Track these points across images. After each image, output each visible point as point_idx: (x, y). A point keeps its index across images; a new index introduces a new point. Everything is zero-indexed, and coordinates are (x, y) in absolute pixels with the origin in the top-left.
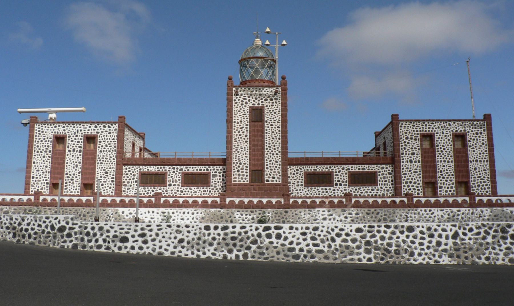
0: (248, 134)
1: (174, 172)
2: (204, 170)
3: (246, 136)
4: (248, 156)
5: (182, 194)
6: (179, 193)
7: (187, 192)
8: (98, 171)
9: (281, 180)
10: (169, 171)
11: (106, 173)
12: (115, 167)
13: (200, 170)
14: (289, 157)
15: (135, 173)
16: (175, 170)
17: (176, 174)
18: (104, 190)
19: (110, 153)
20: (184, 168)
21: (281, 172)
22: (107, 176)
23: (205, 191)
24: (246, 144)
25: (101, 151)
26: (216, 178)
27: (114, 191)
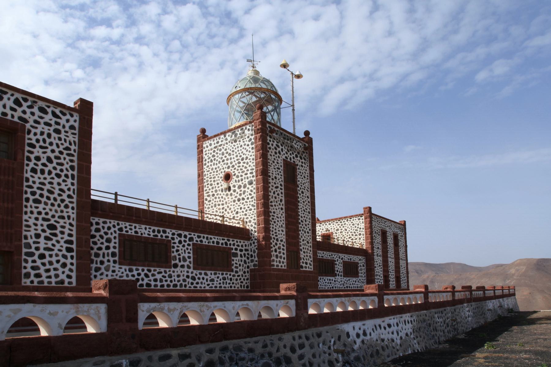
0: (283, 198)
1: (180, 242)
2: (222, 244)
3: (281, 201)
4: (284, 230)
7: (201, 280)
8: (29, 219)
9: (312, 267)
11: (52, 227)
12: (74, 216)
14: (92, 197)
15: (109, 236)
16: (183, 239)
18: (48, 271)
19: (60, 180)
21: (312, 256)
22: (55, 235)
23: (224, 279)
24: (282, 211)
25: (34, 171)
26: (237, 258)
27: (74, 275)
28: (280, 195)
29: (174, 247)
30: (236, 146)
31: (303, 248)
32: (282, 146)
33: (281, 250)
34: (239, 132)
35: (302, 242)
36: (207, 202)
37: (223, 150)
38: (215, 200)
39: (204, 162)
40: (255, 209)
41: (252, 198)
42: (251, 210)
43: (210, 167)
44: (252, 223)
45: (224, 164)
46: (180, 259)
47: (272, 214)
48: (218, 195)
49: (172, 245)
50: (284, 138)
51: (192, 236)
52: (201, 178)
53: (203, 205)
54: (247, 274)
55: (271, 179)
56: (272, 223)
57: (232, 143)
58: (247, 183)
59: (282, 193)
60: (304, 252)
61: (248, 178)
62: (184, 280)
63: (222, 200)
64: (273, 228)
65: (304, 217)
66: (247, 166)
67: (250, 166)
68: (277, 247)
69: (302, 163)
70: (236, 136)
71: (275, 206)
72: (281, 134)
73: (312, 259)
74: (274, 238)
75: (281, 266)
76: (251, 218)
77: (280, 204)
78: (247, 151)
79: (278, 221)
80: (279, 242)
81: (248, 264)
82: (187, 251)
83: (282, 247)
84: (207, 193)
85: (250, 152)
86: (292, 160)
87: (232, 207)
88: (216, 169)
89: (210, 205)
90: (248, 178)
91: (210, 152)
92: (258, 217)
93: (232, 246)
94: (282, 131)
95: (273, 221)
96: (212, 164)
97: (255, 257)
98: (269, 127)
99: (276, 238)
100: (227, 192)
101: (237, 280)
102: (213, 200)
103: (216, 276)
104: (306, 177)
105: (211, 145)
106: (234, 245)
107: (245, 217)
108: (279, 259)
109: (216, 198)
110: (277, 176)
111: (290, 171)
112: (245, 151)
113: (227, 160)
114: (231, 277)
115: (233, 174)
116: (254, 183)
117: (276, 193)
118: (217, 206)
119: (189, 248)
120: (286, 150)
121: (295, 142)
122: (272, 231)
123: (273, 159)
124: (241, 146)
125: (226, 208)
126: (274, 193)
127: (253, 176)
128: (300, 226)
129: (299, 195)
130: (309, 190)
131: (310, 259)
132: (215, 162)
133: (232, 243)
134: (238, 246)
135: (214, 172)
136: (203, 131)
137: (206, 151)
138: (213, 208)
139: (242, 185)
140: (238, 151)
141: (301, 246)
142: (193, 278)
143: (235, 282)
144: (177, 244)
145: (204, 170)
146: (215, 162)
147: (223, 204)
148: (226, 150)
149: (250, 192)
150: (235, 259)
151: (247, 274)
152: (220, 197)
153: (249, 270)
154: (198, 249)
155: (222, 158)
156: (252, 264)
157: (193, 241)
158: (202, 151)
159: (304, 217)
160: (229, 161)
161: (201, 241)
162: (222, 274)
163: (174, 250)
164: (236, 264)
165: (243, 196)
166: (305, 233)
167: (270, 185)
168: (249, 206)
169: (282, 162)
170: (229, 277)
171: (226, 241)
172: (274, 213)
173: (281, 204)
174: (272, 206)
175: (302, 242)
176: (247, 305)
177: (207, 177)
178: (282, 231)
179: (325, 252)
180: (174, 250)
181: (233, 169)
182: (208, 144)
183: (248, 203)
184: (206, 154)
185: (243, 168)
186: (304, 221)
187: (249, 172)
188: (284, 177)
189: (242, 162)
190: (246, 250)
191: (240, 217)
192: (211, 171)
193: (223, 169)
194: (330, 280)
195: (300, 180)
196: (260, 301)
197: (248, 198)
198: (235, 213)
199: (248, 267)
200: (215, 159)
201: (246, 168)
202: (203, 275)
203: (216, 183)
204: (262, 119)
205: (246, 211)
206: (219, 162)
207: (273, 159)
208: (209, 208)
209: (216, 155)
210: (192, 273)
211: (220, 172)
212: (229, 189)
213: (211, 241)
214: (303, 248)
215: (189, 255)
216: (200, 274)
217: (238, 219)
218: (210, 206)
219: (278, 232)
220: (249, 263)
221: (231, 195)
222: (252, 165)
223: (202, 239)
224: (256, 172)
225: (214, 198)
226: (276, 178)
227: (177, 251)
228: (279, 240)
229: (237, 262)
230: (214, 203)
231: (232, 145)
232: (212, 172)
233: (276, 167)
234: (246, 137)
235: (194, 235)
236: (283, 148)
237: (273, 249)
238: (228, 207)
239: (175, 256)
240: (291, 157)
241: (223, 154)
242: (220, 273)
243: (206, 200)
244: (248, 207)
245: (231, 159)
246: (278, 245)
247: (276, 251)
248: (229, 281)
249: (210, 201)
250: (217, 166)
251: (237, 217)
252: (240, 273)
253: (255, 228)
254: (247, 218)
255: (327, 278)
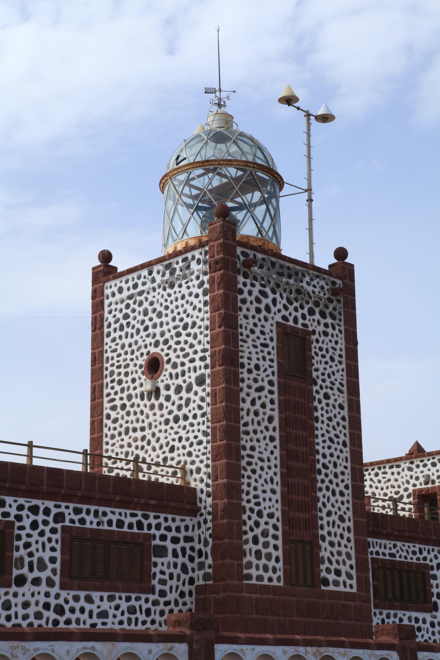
0: (276, 414)
1: (34, 525)
2: (131, 526)
3: (271, 419)
4: (278, 489)
5: (62, 619)
6: (52, 615)
7: (78, 614)
9: (354, 582)
10: (19, 518)
13: (120, 524)
16: (41, 517)
17: (42, 534)
20: (68, 509)
21: (353, 553)
23: (132, 610)
24: (271, 445)
26: (165, 560)
28: (269, 406)
29: (19, 538)
30: (173, 297)
31: (329, 534)
32: (274, 292)
33: (270, 539)
34: (178, 264)
35: (326, 519)
36: (109, 423)
37: (146, 305)
38: (126, 418)
39: (106, 330)
40: (208, 442)
41: (203, 415)
42: (200, 443)
43: (118, 341)
44: (202, 475)
45: (148, 336)
46: (31, 565)
47: (248, 452)
48: (132, 406)
49: (17, 532)
50: (281, 274)
51: (63, 509)
52: (97, 366)
53: (102, 430)
54: (187, 599)
55: (245, 370)
56: (246, 474)
57: (165, 289)
58: (193, 380)
59: (272, 402)
60: (332, 544)
61: (195, 370)
62: (38, 615)
63: (141, 418)
64: (249, 485)
65: (332, 455)
66: (195, 342)
67: (200, 342)
68: (258, 531)
69: (326, 325)
70: (172, 273)
71: (255, 432)
72: (273, 264)
73: (353, 562)
74: (252, 510)
75: (270, 580)
76: (201, 462)
77: (267, 428)
78: (194, 308)
79: (262, 469)
80: (265, 518)
81: (191, 574)
82: (48, 546)
83: (272, 531)
84: (110, 401)
85: (200, 310)
86: (301, 321)
87: (162, 435)
88: (130, 345)
89: (115, 429)
90: (195, 371)
91: (119, 306)
92: (213, 460)
93: (153, 531)
94: (274, 259)
95: (249, 468)
96: (123, 334)
97: (207, 557)
98: (243, 253)
99: (256, 508)
100: (153, 400)
101: (162, 613)
102: (123, 418)
103: (113, 604)
104: (337, 358)
105: (120, 290)
106: (158, 527)
107: (189, 459)
108: (264, 561)
109: (128, 414)
110: (261, 363)
111: (294, 347)
112: (190, 309)
113: (155, 326)
114: (149, 605)
115: (166, 359)
116: (208, 381)
117: (258, 403)
118: (131, 433)
119: (54, 537)
120: (284, 301)
121: (307, 279)
122: (248, 493)
123: (251, 326)
124: (183, 297)
125: (149, 437)
126: (253, 403)
127: (206, 367)
128: (319, 478)
129: (316, 403)
130: (345, 389)
131: (348, 562)
132: (130, 330)
133: (154, 522)
134: (168, 529)
135: (126, 353)
136: (106, 257)
137: (110, 305)
138: (123, 436)
139: (184, 386)
140: (177, 307)
141: (322, 527)
142: (60, 610)
143: (158, 618)
144: (28, 530)
145: (106, 347)
146: (130, 330)
147: (143, 429)
148: (152, 303)
149: (198, 402)
150: (159, 560)
151: (187, 599)
152: (138, 410)
153: (193, 588)
154: (75, 541)
155: (143, 322)
156: (201, 573)
157: (64, 521)
158: (102, 303)
159: (332, 455)
160: (158, 330)
161: (82, 521)
162: (128, 599)
163: (21, 543)
164: (162, 573)
165: (185, 410)
166: (334, 494)
167: (243, 385)
168: (196, 433)
169: (274, 328)
170: (145, 606)
171: (139, 518)
172: (253, 449)
173: (271, 427)
174: (247, 433)
175: (326, 519)
176: (93, 648)
177: (112, 365)
178: (273, 492)
179: (399, 544)
180: (21, 543)
181: (165, 347)
182: (115, 289)
183: (196, 428)
184: (110, 312)
185: (187, 347)
186: (331, 466)
187: (197, 357)
188: (278, 363)
189: (184, 333)
190: (188, 539)
191: (177, 459)
192: (119, 351)
193: (145, 346)
194: (417, 620)
195: (321, 367)
196: (116, 644)
197: (195, 416)
198: (166, 449)
199: (192, 581)
200: (128, 324)
201: (192, 346)
202: (82, 603)
203: (130, 378)
204: (225, 238)
205: (191, 445)
206: (138, 331)
207: (251, 326)
208: (113, 437)
209: (132, 315)
210: (57, 596)
211: (137, 354)
212: (157, 392)
213: (105, 519)
214: (329, 534)
215: (54, 554)
216: (76, 599)
217: (174, 463)
218: (116, 433)
219: (262, 495)
220: (193, 570)
221: (161, 407)
222: (203, 342)
223: (84, 515)
224: (212, 356)
225: (124, 413)
226: (257, 367)
227: (27, 545)
228: (265, 513)
229: (165, 568)
230: (125, 425)
231: (165, 293)
232: (122, 352)
233: (258, 343)
234: (193, 277)
235: (67, 507)
236: (278, 296)
237: (250, 535)
238: (154, 435)
239: (21, 559)
240: (297, 317)
241: (146, 313)
242: (124, 595)
243: (108, 417)
244: (196, 437)
245: (162, 324)
246: (263, 526)
247: (255, 541)
248: (142, 617)
249: (115, 421)
250: (132, 341)
251: (172, 459)
252: (171, 597)
253: (208, 485)
254: (193, 463)
255: (408, 614)
